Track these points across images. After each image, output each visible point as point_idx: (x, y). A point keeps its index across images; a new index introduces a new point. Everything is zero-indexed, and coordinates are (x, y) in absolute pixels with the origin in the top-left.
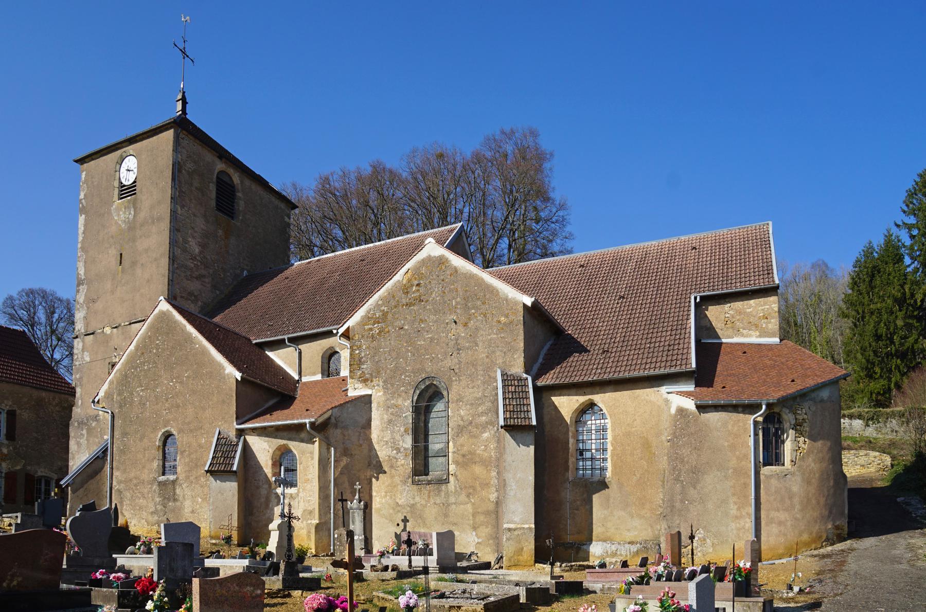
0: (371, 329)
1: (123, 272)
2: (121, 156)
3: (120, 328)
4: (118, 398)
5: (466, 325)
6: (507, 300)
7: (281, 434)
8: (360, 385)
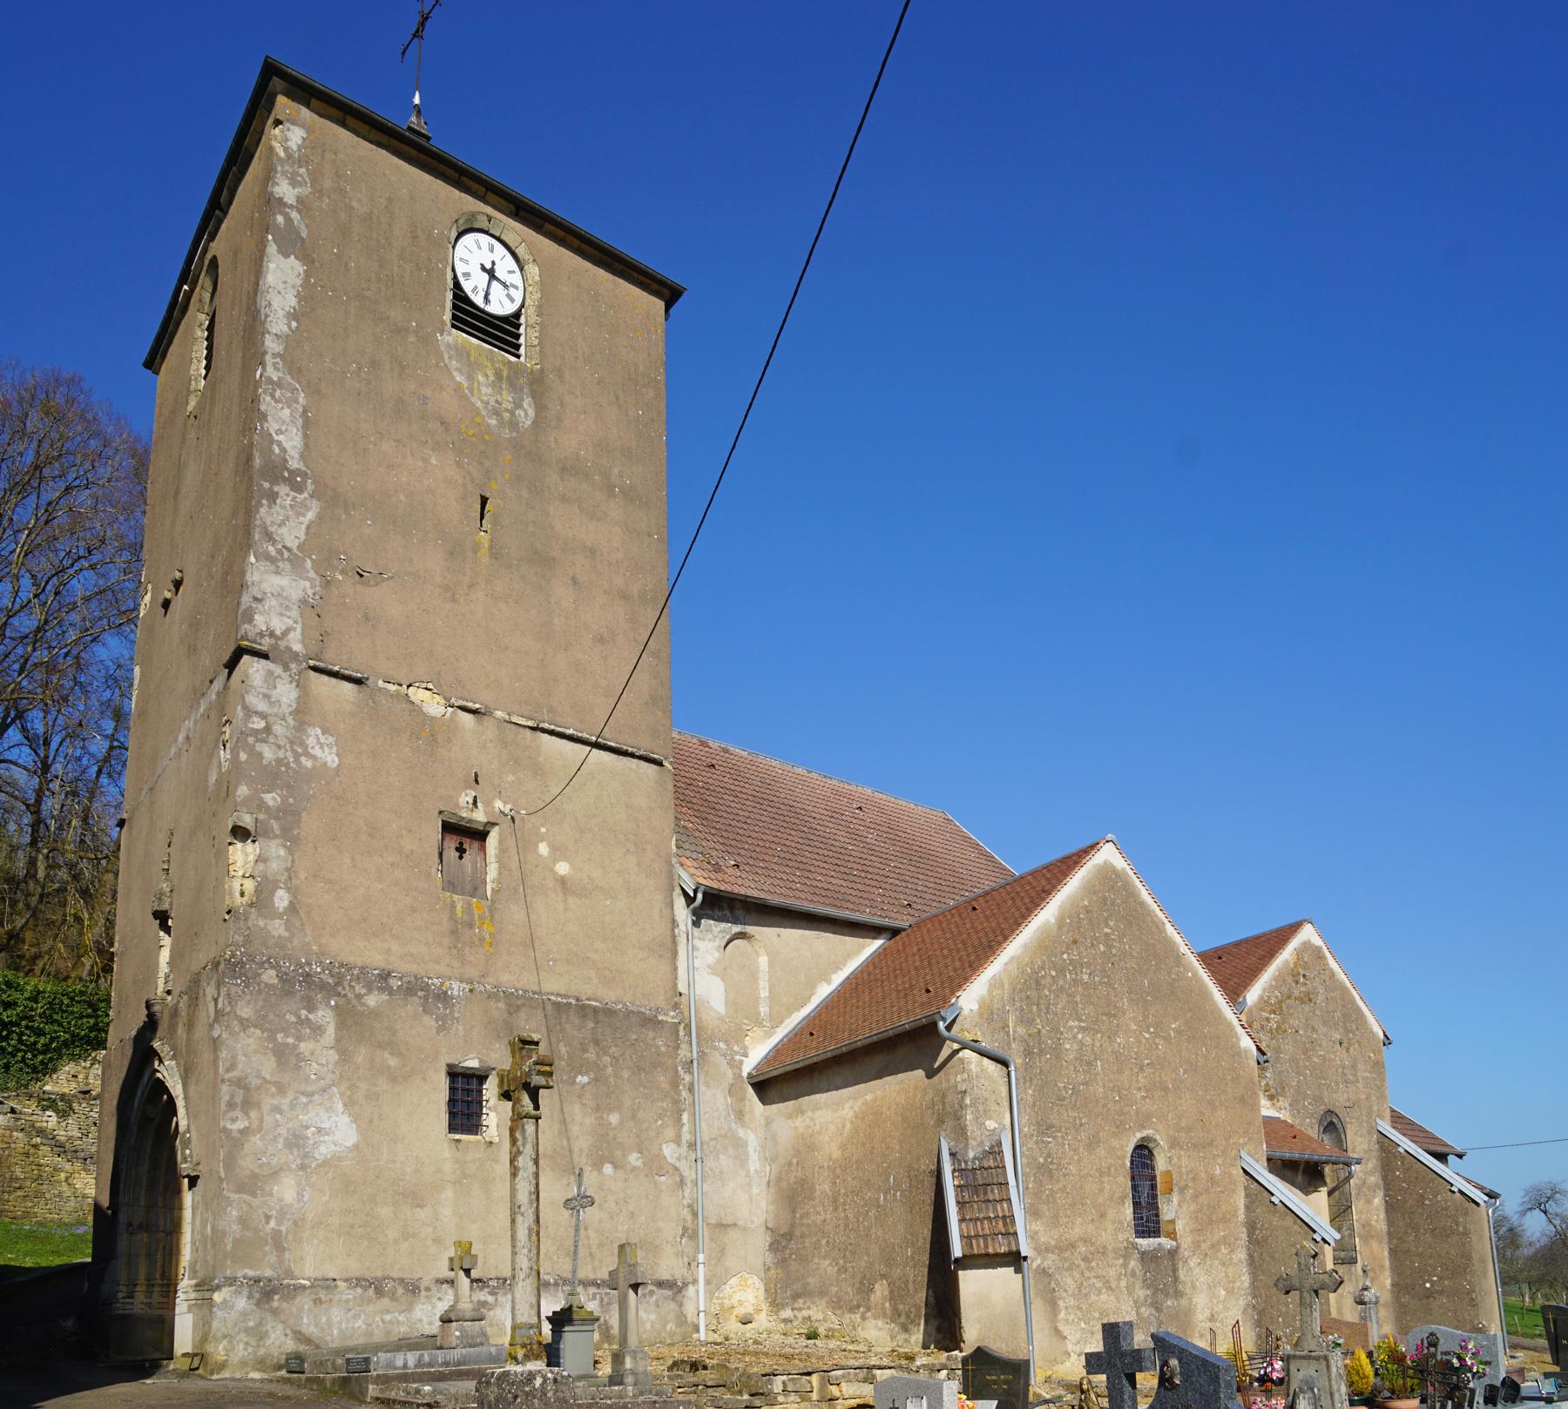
1: (495, 552)
2: (473, 216)
3: (487, 721)
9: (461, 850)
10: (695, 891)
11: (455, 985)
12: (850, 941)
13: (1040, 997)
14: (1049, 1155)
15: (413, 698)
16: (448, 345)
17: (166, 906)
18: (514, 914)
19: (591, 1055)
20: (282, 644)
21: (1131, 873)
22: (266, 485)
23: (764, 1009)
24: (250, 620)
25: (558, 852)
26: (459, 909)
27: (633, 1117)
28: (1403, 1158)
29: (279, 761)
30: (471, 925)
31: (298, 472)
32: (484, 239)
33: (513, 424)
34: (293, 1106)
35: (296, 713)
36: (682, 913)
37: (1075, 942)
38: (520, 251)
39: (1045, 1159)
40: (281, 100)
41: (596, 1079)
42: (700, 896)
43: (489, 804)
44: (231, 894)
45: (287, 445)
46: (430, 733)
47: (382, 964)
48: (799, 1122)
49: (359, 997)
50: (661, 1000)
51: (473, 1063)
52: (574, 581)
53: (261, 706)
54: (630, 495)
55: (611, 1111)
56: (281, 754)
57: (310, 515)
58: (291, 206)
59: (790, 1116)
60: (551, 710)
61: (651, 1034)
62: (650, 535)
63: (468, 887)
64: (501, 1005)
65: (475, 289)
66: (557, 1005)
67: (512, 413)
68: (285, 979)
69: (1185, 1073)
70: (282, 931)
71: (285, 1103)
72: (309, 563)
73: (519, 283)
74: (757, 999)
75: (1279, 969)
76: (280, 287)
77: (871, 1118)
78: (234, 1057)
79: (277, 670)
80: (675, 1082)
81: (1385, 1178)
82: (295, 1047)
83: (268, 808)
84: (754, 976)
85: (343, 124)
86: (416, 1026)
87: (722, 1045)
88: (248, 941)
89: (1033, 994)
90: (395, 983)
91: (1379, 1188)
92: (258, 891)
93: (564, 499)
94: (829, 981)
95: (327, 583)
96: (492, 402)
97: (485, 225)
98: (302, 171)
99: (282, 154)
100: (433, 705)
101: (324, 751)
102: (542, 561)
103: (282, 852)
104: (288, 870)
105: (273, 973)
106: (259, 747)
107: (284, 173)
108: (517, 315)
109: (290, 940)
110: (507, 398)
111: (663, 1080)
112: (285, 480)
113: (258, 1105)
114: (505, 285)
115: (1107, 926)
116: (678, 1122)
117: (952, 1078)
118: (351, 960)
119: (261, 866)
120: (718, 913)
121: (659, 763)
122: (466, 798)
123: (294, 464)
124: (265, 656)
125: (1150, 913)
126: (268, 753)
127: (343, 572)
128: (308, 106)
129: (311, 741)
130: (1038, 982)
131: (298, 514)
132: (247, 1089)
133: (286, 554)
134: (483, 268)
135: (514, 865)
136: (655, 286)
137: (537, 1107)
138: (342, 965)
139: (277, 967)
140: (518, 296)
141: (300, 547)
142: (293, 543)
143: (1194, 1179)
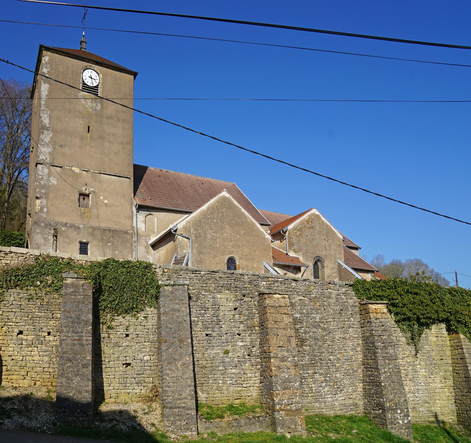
0: (296, 233)
1: (91, 138)
2: (87, 66)
3: (89, 172)
4: (195, 232)
5: (327, 241)
6: (338, 237)
7: (285, 268)
8: (294, 253)
9: (84, 199)
10: (136, 205)
11: (81, 225)
12: (179, 215)
13: (201, 225)
14: (201, 259)
15: (73, 169)
16: (81, 96)
17: (30, 213)
18: (95, 211)
19: (111, 239)
20: (45, 161)
21: (231, 197)
22: (42, 131)
23: (156, 230)
24: (39, 157)
25: (105, 198)
26: (82, 210)
27: (121, 252)
28: (344, 269)
29: (45, 184)
30: (85, 214)
31: (48, 127)
32: (90, 70)
33: (96, 110)
34: (47, 248)
35: (48, 174)
36: (134, 210)
37: (212, 213)
38: (98, 72)
39: (200, 259)
40: (44, 51)
41: (112, 244)
42: (137, 206)
43: (89, 189)
44: (36, 209)
45: (46, 122)
46: (77, 176)
47: (66, 222)
48: (158, 254)
49: (61, 228)
50: (129, 228)
51: (85, 241)
52: (110, 141)
53: (41, 174)
54: (124, 121)
55: (116, 251)
56: (45, 183)
57: (51, 135)
58: (46, 73)
59: (157, 253)
60: (104, 169)
61: (126, 235)
62: (129, 129)
63: (85, 206)
64: (91, 229)
65: (88, 82)
66: (104, 229)
67: (95, 107)
68: (46, 225)
69: (246, 242)
70: (45, 216)
71: (46, 248)
72: (50, 145)
73: (98, 78)
74: (154, 228)
75: (301, 220)
76: (44, 90)
77: (167, 251)
78: (36, 239)
79: (44, 166)
80: (132, 245)
81: (339, 275)
82: (48, 237)
83: (42, 193)
84: (154, 223)
85: (57, 54)
86: (73, 234)
87: (144, 238)
88: (39, 218)
89: (199, 224)
90: (68, 225)
91: (337, 277)
92: (41, 208)
93: (108, 124)
94: (173, 224)
95: (54, 148)
96: (91, 106)
97: (90, 67)
98: (48, 65)
99: (44, 63)
100: (77, 170)
101: (54, 181)
102: (102, 138)
103: (45, 201)
104: (47, 204)
105: (43, 224)
106: (41, 181)
107: (45, 67)
108: (98, 85)
109: (47, 218)
110: (94, 105)
111: (128, 245)
112: (45, 129)
113: (40, 248)
114: (94, 79)
115: (223, 210)
116: (132, 254)
117: (177, 242)
118: (59, 221)
119: (41, 204)
120: (144, 209)
121: (130, 178)
122: (84, 189)
123: (47, 126)
124: (42, 164)
125: (237, 207)
126: (42, 182)
127: (57, 146)
128: (49, 51)
129: (51, 179)
130: (200, 222)
131: (48, 135)
132: (38, 245)
133: (46, 144)
134: (89, 77)
135: (95, 201)
136: (131, 73)
137: (57, 239)
138: (57, 222)
139: (44, 223)
140: (98, 81)
141: (49, 142)
142: (47, 141)
143: (247, 267)
